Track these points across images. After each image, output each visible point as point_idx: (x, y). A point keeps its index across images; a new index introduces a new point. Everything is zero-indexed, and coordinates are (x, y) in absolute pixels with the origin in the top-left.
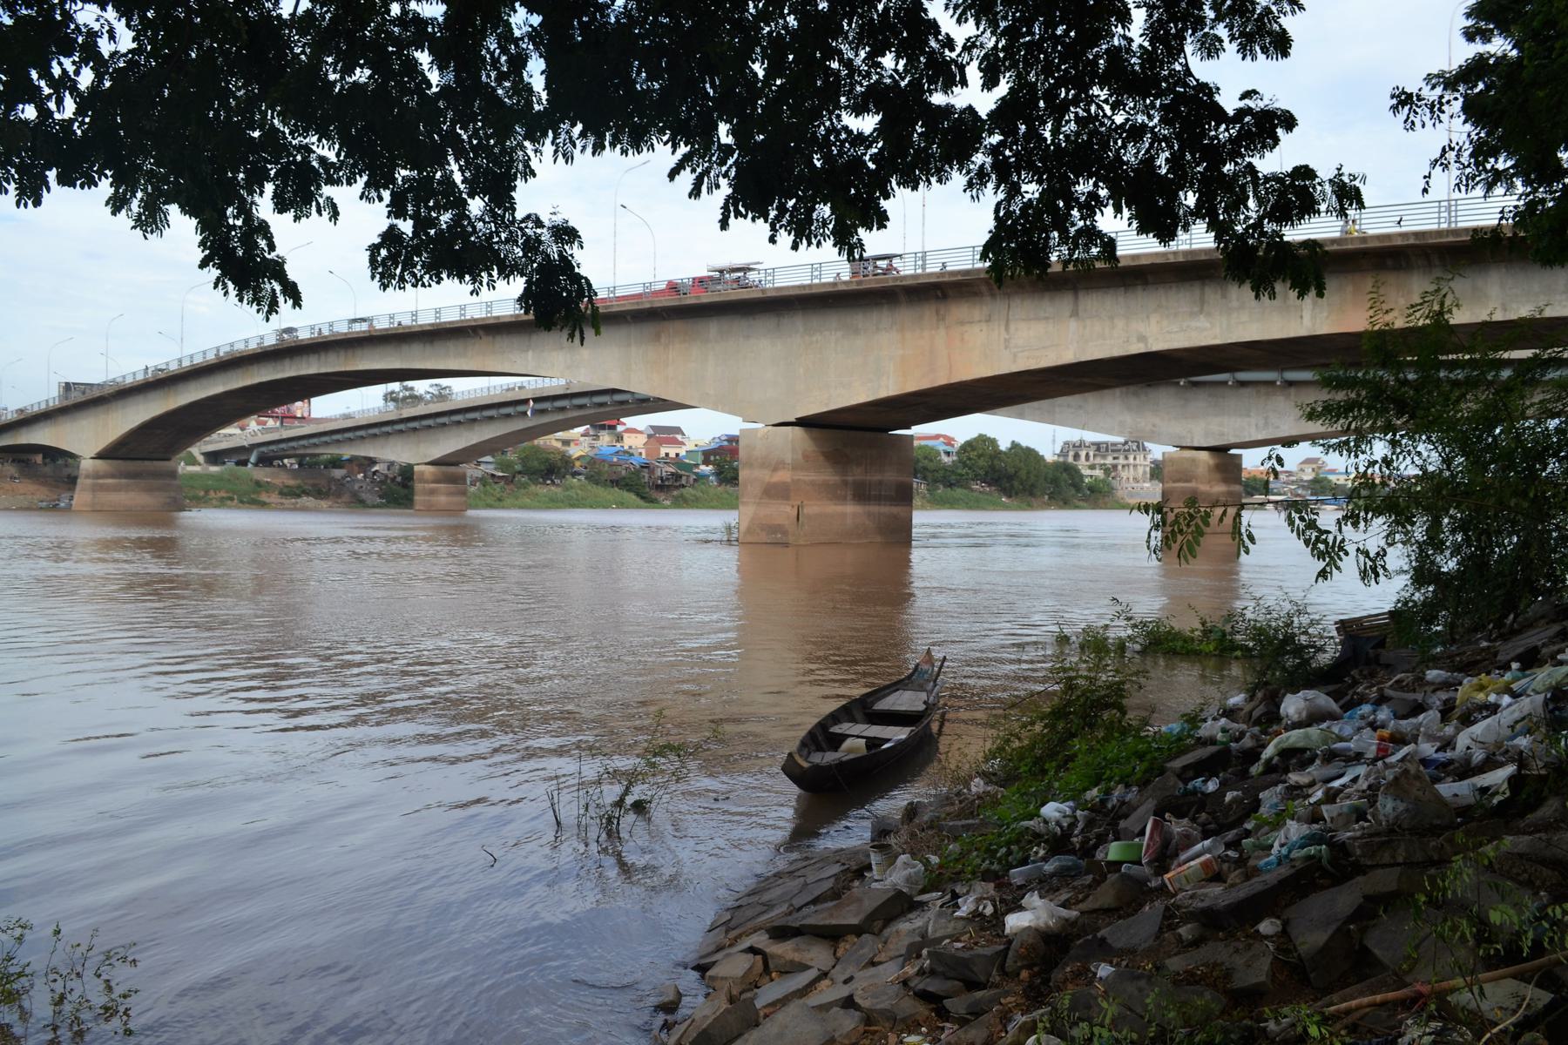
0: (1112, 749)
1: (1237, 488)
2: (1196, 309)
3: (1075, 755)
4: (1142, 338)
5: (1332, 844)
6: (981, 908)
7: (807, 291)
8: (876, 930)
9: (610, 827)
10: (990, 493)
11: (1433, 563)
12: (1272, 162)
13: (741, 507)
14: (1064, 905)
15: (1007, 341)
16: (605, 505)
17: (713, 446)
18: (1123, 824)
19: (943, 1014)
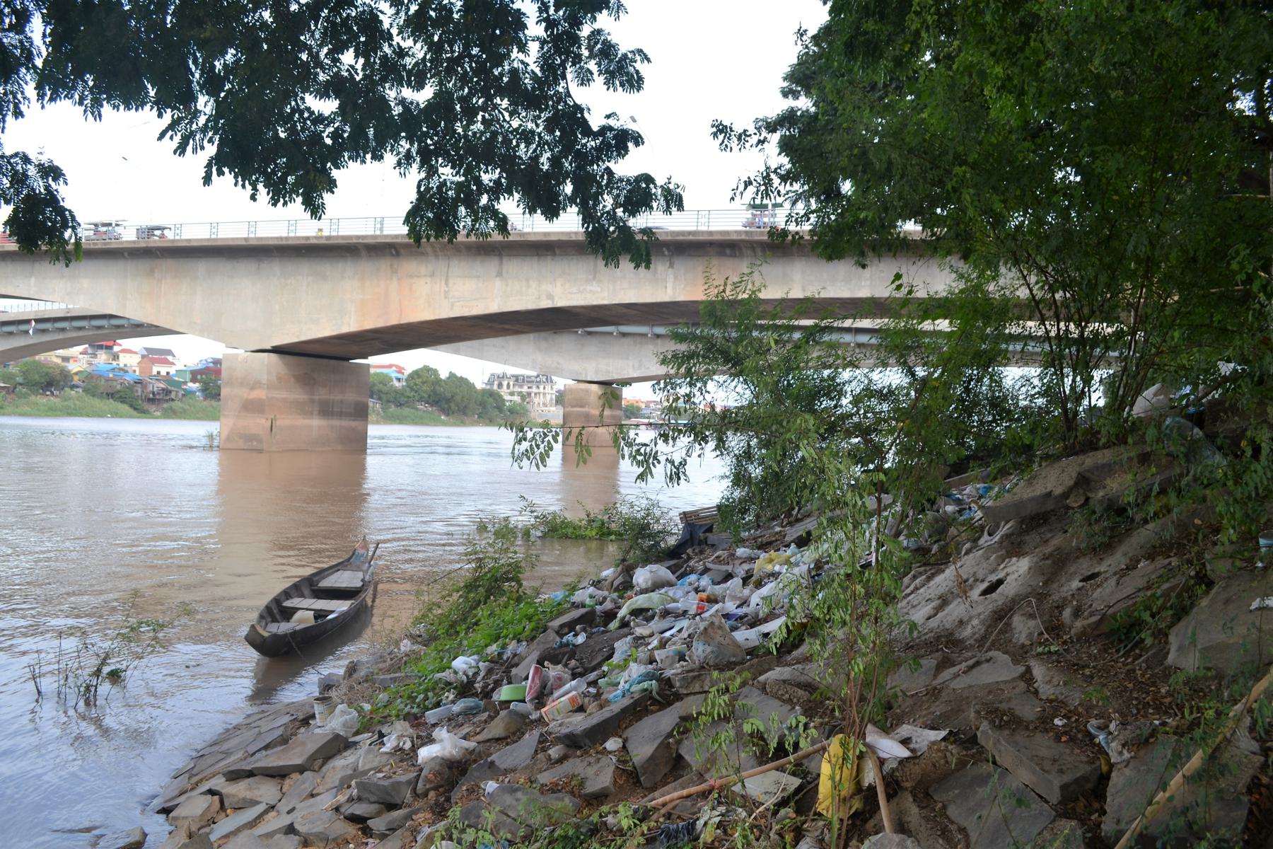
0: (508, 614)
1: (618, 413)
2: (591, 277)
3: (479, 620)
4: (550, 297)
5: (660, 680)
6: (401, 744)
7: (284, 242)
8: (316, 768)
9: (89, 696)
10: (431, 413)
11: (746, 470)
12: (626, 167)
13: (222, 418)
14: (464, 738)
15: (446, 292)
16: (100, 415)
17: (200, 366)
18: (514, 671)
19: (367, 832)
